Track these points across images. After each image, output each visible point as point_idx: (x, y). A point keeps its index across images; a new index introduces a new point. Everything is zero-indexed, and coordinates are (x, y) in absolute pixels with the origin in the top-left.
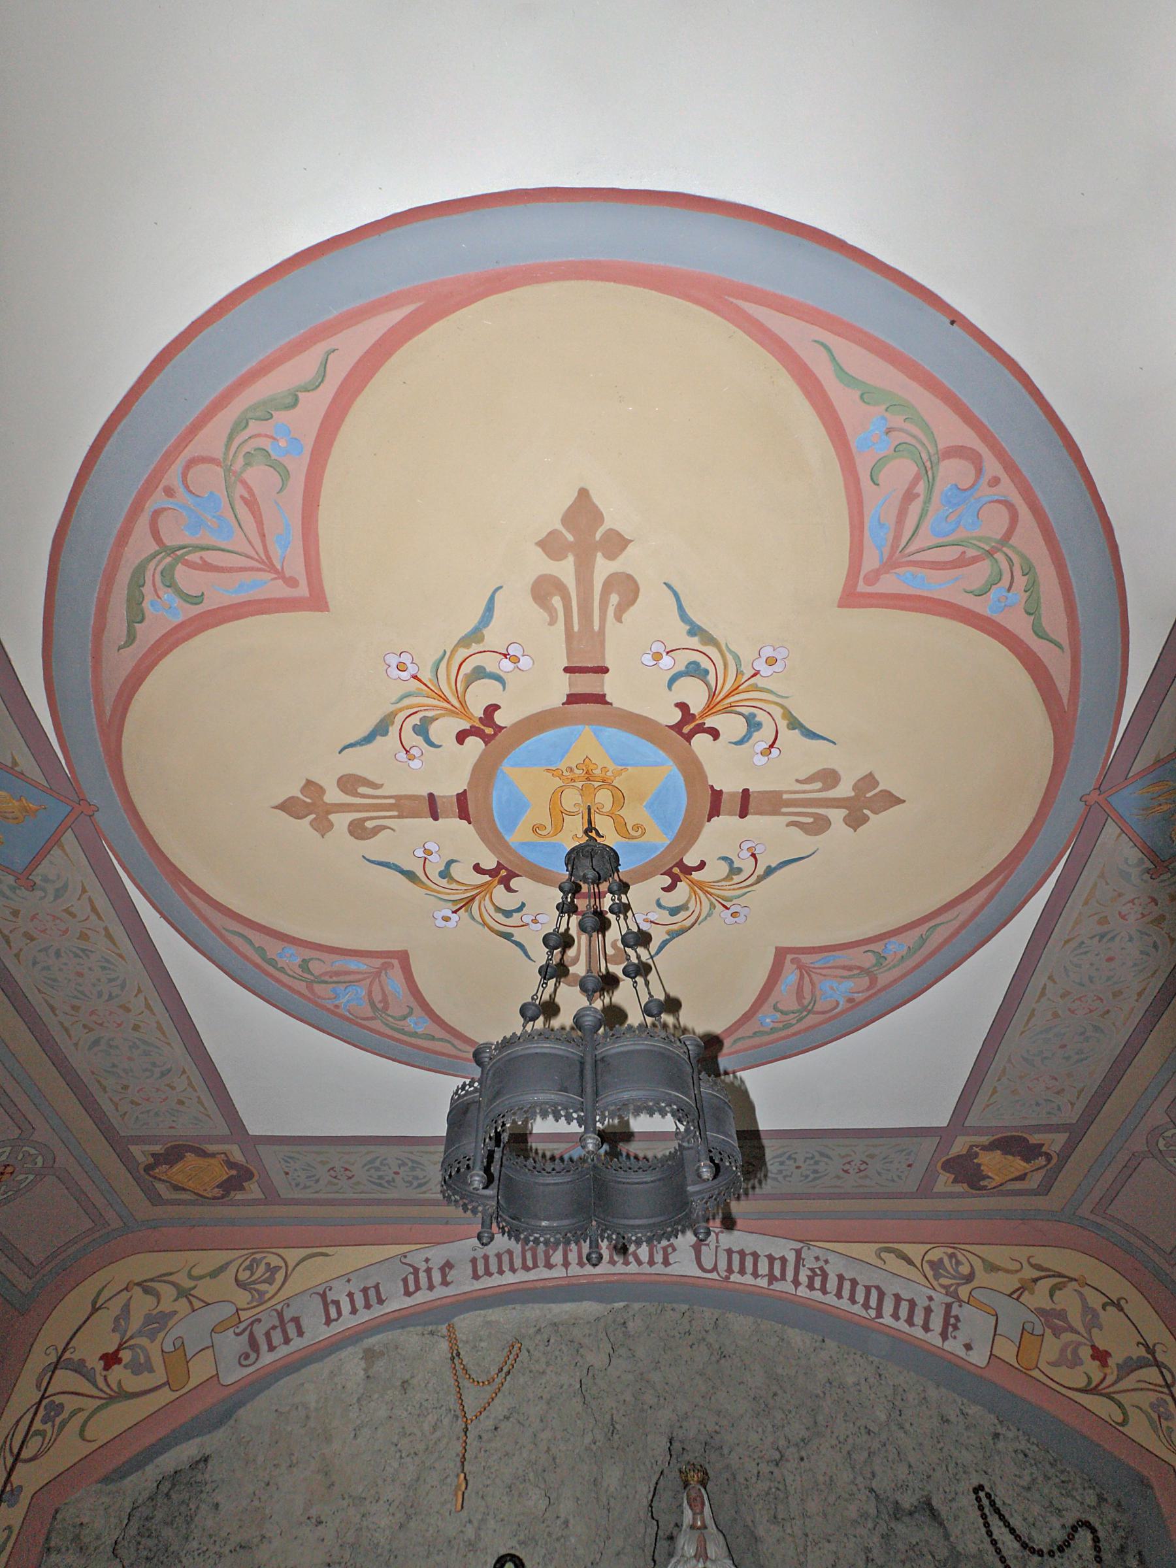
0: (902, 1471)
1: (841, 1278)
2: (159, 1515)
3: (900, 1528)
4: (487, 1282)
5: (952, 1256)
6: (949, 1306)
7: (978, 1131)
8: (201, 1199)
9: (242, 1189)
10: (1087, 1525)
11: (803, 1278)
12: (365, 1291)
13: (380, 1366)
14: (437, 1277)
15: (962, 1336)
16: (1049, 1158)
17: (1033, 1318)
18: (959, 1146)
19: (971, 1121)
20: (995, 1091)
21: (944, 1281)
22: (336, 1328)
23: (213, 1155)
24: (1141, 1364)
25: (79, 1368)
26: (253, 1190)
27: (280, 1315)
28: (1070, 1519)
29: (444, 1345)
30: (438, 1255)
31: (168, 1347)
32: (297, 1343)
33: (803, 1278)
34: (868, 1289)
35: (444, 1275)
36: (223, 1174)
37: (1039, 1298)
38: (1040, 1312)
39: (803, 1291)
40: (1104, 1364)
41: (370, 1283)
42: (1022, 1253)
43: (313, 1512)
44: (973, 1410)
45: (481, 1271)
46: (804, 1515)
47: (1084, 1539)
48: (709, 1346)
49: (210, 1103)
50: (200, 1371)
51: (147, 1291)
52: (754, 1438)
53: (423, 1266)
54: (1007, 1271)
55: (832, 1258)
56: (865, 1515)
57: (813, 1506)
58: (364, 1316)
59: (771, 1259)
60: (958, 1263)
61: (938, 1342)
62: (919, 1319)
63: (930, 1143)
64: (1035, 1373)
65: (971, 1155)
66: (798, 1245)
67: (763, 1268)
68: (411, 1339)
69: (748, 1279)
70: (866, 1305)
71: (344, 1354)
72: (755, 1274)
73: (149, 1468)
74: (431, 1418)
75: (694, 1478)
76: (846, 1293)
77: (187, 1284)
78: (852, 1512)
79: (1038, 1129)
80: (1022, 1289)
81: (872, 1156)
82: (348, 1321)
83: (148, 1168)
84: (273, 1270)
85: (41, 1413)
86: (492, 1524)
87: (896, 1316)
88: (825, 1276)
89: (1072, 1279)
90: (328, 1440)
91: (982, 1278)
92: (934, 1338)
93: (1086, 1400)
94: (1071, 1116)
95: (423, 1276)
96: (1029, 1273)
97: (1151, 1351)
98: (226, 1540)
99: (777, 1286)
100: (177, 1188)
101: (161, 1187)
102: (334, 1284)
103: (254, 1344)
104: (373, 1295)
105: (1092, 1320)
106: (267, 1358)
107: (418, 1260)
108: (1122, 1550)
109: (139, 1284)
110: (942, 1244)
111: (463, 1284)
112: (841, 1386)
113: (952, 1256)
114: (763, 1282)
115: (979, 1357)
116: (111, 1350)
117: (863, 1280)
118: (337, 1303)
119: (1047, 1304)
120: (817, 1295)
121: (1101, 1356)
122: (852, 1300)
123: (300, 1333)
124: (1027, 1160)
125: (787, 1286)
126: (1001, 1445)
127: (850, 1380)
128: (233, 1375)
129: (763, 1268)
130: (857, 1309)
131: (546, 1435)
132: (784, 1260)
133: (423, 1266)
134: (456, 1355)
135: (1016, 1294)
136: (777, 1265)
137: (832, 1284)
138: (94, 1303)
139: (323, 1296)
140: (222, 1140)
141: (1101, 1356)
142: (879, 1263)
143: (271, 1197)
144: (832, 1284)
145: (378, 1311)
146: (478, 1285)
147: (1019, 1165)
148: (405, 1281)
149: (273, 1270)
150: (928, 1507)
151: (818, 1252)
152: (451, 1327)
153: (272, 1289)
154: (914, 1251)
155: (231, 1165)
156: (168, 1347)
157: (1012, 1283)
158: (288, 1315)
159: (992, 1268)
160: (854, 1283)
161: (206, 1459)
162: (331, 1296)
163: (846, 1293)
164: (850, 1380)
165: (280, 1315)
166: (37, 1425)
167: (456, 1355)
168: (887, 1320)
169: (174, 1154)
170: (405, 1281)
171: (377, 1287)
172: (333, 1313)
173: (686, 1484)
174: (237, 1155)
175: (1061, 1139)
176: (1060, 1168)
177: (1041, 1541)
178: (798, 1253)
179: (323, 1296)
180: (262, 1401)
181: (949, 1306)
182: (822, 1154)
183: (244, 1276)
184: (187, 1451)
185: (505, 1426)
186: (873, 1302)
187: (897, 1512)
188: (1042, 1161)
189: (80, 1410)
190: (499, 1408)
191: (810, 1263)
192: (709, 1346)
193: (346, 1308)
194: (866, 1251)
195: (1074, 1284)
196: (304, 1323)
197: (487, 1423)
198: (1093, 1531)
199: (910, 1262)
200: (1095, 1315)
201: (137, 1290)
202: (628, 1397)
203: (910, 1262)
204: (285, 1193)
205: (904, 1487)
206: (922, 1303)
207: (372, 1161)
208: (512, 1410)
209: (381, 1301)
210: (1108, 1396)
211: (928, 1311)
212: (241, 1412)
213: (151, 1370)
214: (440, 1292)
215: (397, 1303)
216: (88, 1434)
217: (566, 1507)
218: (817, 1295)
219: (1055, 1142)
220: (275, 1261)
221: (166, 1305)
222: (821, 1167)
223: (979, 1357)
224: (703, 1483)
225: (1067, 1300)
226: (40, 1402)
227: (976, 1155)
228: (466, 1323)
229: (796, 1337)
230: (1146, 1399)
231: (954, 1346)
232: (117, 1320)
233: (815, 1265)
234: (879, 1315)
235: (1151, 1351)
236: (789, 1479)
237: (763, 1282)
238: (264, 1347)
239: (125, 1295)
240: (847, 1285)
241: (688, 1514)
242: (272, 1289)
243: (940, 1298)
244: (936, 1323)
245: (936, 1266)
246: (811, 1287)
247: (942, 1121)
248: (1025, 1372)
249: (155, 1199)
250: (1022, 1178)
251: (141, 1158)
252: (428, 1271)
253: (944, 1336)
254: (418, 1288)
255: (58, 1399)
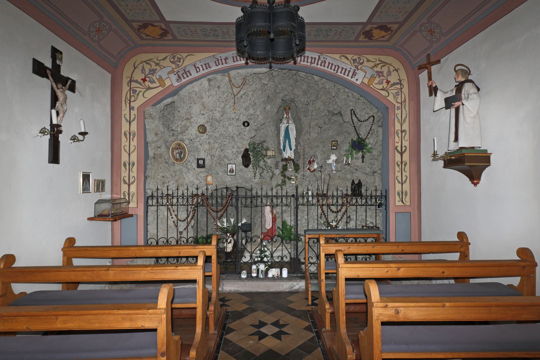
0: (336, 107)
1: (329, 63)
2: (166, 113)
3: (333, 118)
4: (237, 63)
5: (359, 58)
6: (355, 70)
7: (374, 23)
8: (154, 39)
9: (166, 36)
10: (373, 116)
11: (319, 63)
12: (205, 64)
13: (212, 83)
14: (224, 62)
15: (356, 78)
16: (392, 31)
17: (375, 73)
18: (368, 28)
19: (373, 21)
20: (382, 12)
21: (355, 64)
22: (199, 74)
23: (156, 26)
24: (397, 84)
25: (136, 81)
26: (170, 37)
27: (184, 70)
28: (370, 115)
29: (227, 78)
30: (223, 55)
31: (158, 78)
32: (190, 77)
33: (319, 63)
34: (335, 66)
35: (226, 61)
36: (161, 32)
37: (378, 69)
38: (377, 72)
39: (319, 66)
40: (388, 84)
41: (206, 63)
42: (377, 57)
43: (202, 112)
44: (355, 94)
45: (235, 60)
46: (312, 115)
47: (372, 118)
48: (294, 79)
49: (153, 10)
50: (168, 83)
51: (147, 63)
52: (302, 100)
53: (220, 59)
54: (372, 62)
55: (328, 58)
56: (325, 115)
57: (314, 113)
58: (206, 71)
59: (312, 58)
60: (360, 59)
61: (350, 79)
62: (346, 73)
63: (360, 27)
64: (371, 86)
65: (371, 30)
66: (319, 54)
67: (309, 60)
68: (219, 77)
69: (305, 63)
70: (334, 70)
71: (203, 80)
72: (307, 62)
73: (161, 104)
74: (226, 94)
75: (287, 108)
76: (330, 67)
77: (158, 62)
78: (323, 114)
79: (392, 23)
80: (375, 66)
81: (343, 30)
82: (202, 72)
83: (138, 30)
84: (180, 59)
85: (132, 92)
86: (242, 115)
87: (341, 73)
88: (325, 62)
89: (388, 64)
90: (202, 98)
91: (365, 63)
92: (349, 78)
93: (381, 92)
94: (401, 19)
95: (220, 61)
96: (378, 62)
97: (400, 81)
98: (183, 118)
99: (312, 65)
100: (147, 35)
101: (143, 35)
102: (197, 63)
103: (180, 78)
104: (208, 66)
105: (389, 73)
106: (184, 81)
107: (218, 56)
108: (379, 121)
109: (144, 62)
110: (357, 54)
111: (231, 63)
112: (325, 89)
113: (359, 58)
114: (309, 64)
115: (359, 82)
116: (143, 78)
117: (335, 64)
118: (199, 68)
119: (379, 70)
120: (322, 67)
121: (388, 82)
122: (331, 69)
123: (191, 75)
124: (386, 32)
125: (315, 65)
126: (359, 101)
127: (327, 87)
128: (176, 84)
129: (309, 60)
130: (332, 71)
131: (253, 98)
132: (315, 58)
133: (220, 59)
134: (230, 81)
135: (372, 68)
136: (313, 60)
137: (327, 65)
138: (134, 66)
139: (195, 66)
140: (158, 22)
141: (388, 82)
142: (340, 59)
143: (175, 38)
144: (327, 65)
145: (209, 70)
146: (235, 64)
147: (383, 33)
148: (215, 62)
149: (180, 59)
150: (340, 113)
151: (324, 56)
152: (229, 74)
153: (180, 64)
154: (349, 56)
155: (162, 29)
156: (158, 78)
157: (373, 64)
158: (186, 70)
159: (368, 61)
160: (332, 64)
161: (174, 102)
162: (197, 66)
163: (330, 67)
164: (327, 87)
165: (184, 70)
166: (132, 94)
167: (230, 81)
168: (339, 73)
169: (145, 25)
170: (215, 62)
171: (208, 64)
172: (198, 70)
173: (285, 109)
174: (164, 27)
175: (397, 26)
176: (395, 34)
177: (362, 119)
178: (319, 56)
179: (195, 66)
180: (184, 90)
181: (355, 70)
182: (330, 30)
183: (172, 60)
184: (169, 100)
185: (244, 96)
186: (336, 69)
187: (334, 114)
188: (390, 32)
189: (141, 91)
190: (242, 93)
191: (322, 59)
192: (294, 79)
193: (201, 69)
194: (337, 56)
195: (388, 65)
196: (191, 72)
197: (239, 96)
198: (374, 119)
199: (348, 59)
200: (390, 72)
201: (144, 63)
202: (273, 90)
203: (348, 59)
204: (179, 37)
205: (335, 110)
206: (348, 69)
207: (203, 29)
208: (245, 93)
209: (210, 67)
210: (386, 91)
211: (349, 71)
212: (180, 92)
213: (155, 83)
214: (225, 65)
215: (214, 68)
216: (145, 95)
217: (258, 113)
218: (322, 67)
219: (394, 27)
220: (180, 57)
221: (154, 67)
222: (329, 33)
223: (359, 82)
224: (289, 109)
225: (385, 70)
226: (130, 90)
227: (372, 30)
228: (233, 73)
229: (316, 78)
230: (394, 92)
231: (354, 80)
232: (142, 70)
233: (323, 60)
234: (337, 72)
235: (400, 81)
236: (310, 108)
237: (309, 64)
238: (182, 78)
239: (141, 65)
240: (330, 65)
241: (285, 115)
242: (180, 64)
243: (353, 68)
244: (351, 74)
245: (354, 60)
246: (321, 65)
247: (365, 20)
248: (369, 86)
249: (142, 39)
250: (383, 37)
251: (136, 27)
252: (221, 60)
253: (352, 77)
254: (314, 63)
255: (135, 89)
